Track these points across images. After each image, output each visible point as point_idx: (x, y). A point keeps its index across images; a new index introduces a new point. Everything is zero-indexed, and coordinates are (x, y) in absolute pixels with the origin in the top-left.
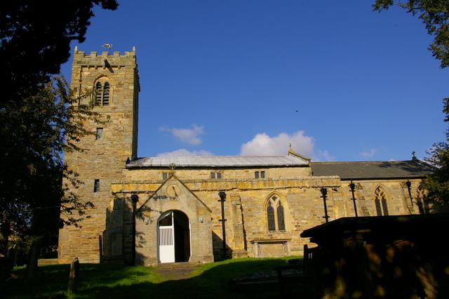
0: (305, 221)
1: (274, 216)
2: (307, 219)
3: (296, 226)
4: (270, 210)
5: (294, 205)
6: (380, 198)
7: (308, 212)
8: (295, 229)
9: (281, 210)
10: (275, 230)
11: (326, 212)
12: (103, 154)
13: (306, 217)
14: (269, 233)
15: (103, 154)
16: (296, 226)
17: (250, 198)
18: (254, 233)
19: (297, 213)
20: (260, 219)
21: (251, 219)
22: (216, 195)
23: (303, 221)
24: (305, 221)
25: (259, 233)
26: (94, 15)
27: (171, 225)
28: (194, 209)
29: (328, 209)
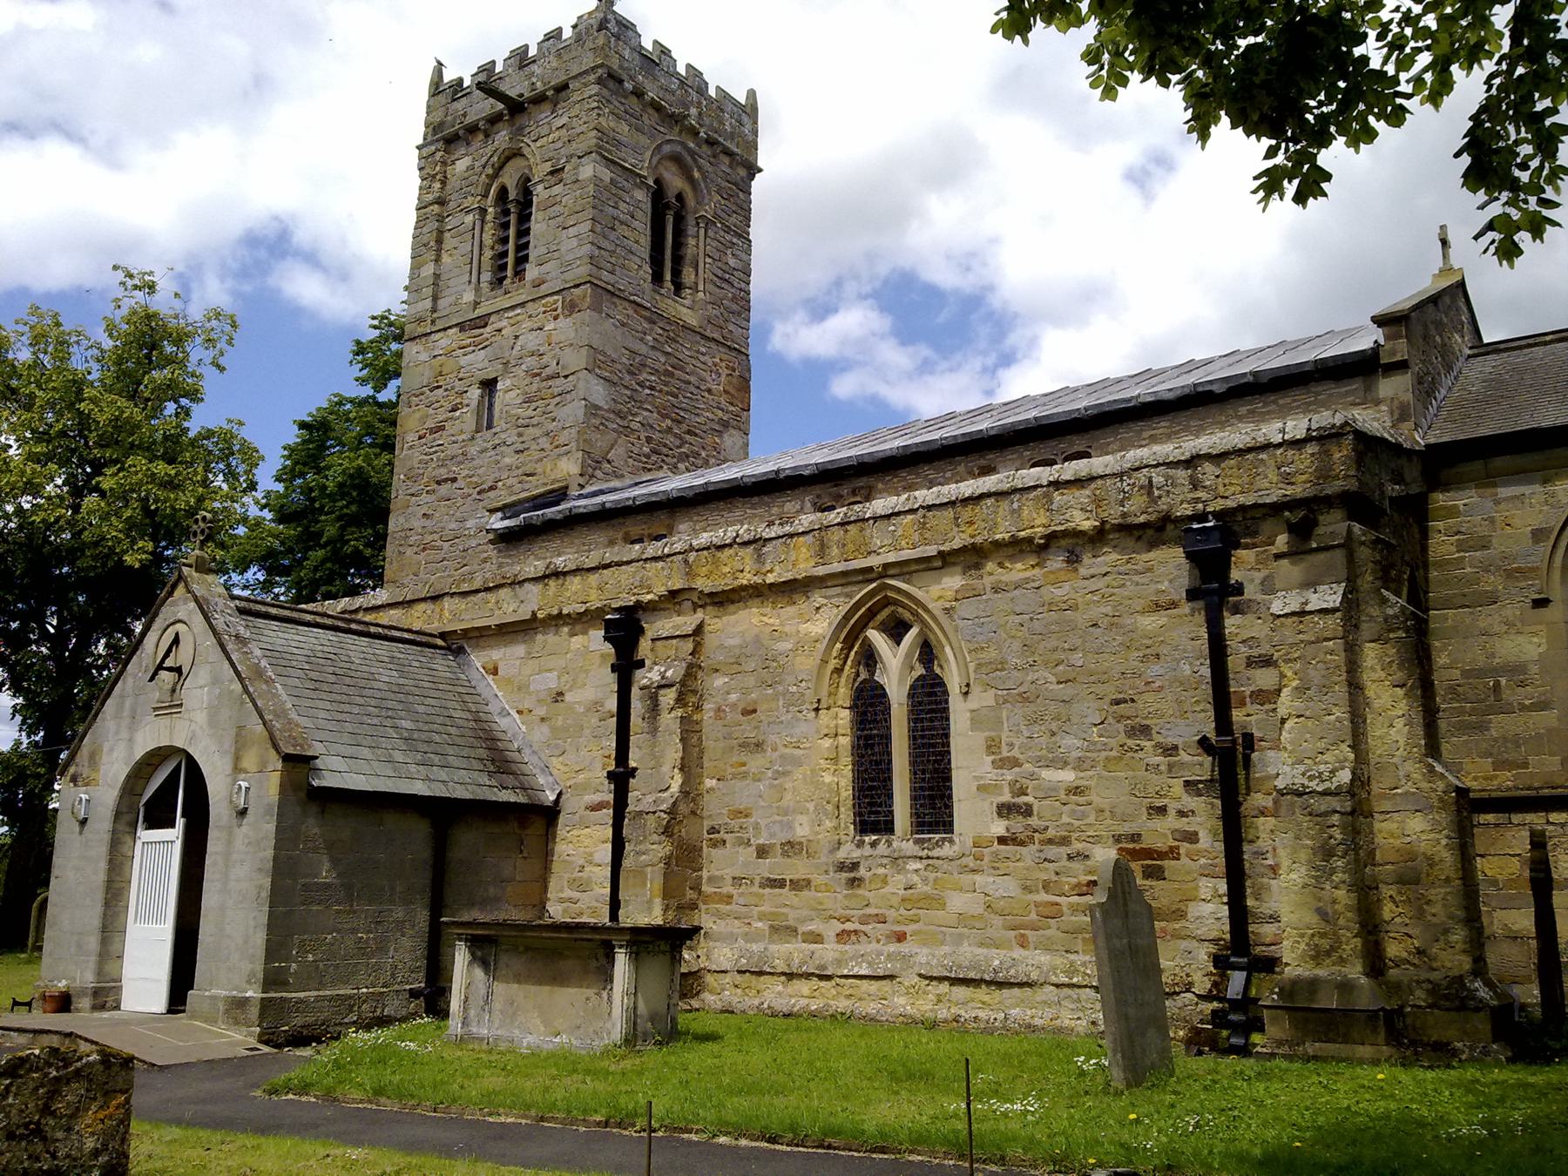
0: (1068, 776)
1: (887, 738)
2: (1080, 764)
3: (1005, 810)
4: (869, 704)
5: (1001, 665)
6: (896, 667)
7: (1090, 710)
8: (999, 828)
9: (930, 698)
10: (888, 828)
11: (1222, 700)
12: (491, 488)
13: (1070, 744)
14: (848, 852)
15: (491, 488)
16: (1005, 810)
17: (757, 639)
18: (762, 852)
19: (1012, 716)
20: (798, 762)
21: (756, 763)
22: (1170, 567)
23: (1050, 775)
24: (1068, 776)
25: (791, 847)
26: (1026, 42)
27: (173, 826)
28: (228, 743)
29: (1243, 681)
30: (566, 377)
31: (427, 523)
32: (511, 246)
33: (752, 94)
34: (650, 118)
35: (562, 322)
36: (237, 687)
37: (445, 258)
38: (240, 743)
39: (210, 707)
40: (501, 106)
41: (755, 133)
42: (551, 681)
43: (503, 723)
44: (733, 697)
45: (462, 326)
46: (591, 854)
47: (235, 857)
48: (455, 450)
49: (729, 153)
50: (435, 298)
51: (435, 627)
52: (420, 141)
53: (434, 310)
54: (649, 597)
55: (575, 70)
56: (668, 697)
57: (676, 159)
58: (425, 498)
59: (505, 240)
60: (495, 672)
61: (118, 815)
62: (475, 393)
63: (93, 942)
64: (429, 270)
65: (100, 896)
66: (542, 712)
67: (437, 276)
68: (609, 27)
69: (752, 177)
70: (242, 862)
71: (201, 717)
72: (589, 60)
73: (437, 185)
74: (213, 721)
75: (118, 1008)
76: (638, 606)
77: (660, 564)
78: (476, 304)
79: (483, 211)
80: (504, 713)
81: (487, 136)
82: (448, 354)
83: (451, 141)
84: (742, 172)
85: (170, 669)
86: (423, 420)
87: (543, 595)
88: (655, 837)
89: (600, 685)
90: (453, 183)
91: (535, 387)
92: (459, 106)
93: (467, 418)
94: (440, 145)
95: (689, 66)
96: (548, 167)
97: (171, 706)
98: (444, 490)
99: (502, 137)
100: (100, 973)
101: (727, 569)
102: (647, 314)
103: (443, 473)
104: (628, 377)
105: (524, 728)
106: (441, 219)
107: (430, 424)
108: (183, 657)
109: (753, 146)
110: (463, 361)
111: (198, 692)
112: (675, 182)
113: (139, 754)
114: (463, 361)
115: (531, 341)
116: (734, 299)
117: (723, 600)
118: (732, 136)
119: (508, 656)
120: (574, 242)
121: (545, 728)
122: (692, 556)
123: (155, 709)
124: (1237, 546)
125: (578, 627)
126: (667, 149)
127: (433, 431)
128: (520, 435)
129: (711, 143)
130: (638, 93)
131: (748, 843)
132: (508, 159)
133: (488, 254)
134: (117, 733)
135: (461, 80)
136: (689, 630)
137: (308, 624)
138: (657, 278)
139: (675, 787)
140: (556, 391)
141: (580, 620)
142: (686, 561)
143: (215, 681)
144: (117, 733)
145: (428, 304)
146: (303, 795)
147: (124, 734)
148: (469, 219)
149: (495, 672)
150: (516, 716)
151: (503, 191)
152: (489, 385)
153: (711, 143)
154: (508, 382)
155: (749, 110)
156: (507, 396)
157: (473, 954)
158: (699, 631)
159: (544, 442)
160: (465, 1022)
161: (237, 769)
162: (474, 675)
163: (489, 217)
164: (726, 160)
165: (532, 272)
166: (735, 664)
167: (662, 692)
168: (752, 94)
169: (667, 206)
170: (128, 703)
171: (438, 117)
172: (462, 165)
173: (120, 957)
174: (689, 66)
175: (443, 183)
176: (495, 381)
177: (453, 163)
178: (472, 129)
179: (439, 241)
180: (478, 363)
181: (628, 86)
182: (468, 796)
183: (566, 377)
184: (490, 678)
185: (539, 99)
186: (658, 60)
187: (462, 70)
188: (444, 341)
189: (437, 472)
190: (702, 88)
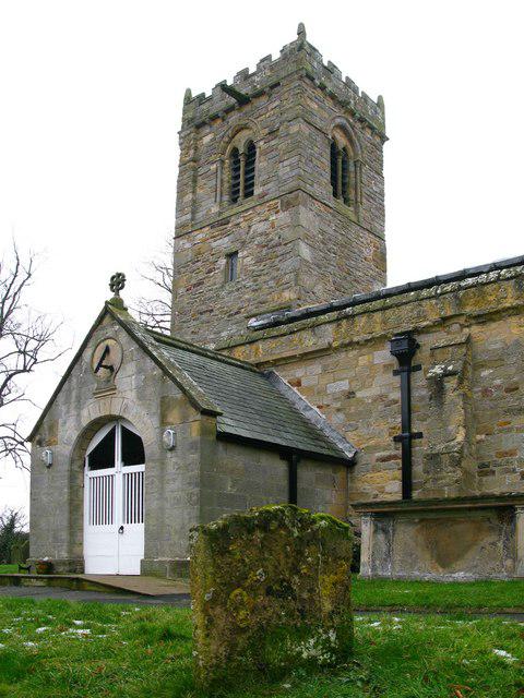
12: (237, 313)
15: (237, 313)
28: (155, 408)
30: (286, 244)
31: (195, 336)
32: (242, 179)
33: (380, 98)
34: (329, 103)
35: (281, 215)
36: (158, 372)
37: (199, 191)
38: (165, 407)
39: (138, 388)
40: (233, 100)
41: (384, 119)
42: (344, 386)
43: (307, 414)
44: (498, 382)
45: (212, 226)
46: (383, 487)
47: (167, 477)
48: (211, 294)
49: (372, 128)
50: (193, 213)
51: (252, 360)
52: (180, 129)
53: (193, 219)
54: (425, 323)
55: (283, 74)
56: (451, 384)
57: (342, 127)
58: (193, 323)
59: (238, 177)
60: (298, 384)
61: (72, 461)
62: (223, 261)
63: (64, 535)
64: (189, 197)
65: (66, 508)
66: (339, 405)
67: (194, 201)
68: (300, 50)
69: (383, 142)
70: (174, 480)
71: (131, 395)
72: (292, 68)
73: (192, 152)
74: (141, 396)
75: (83, 572)
76: (417, 331)
77: (434, 301)
78: (220, 213)
79: (223, 162)
80: (307, 408)
81: (223, 120)
82: (204, 241)
83: (198, 127)
84: (378, 140)
85: (105, 367)
86: (188, 281)
87: (337, 332)
88: (450, 468)
89: (385, 385)
90: (202, 149)
91: (264, 252)
92: (204, 107)
93: (218, 276)
94: (192, 129)
95: (347, 78)
96: (267, 131)
97: (108, 388)
98: (204, 317)
99: (234, 118)
100: (70, 551)
101: (491, 298)
102: (331, 211)
103: (204, 308)
104: (322, 246)
105: (324, 416)
106: (195, 169)
107: (194, 281)
108: (114, 358)
109: (383, 125)
110: (214, 244)
111: (128, 380)
112: (342, 141)
113: (85, 422)
114: (214, 244)
115: (261, 227)
116: (377, 209)
117: (483, 319)
118: (372, 118)
119: (310, 373)
120: (288, 169)
121: (341, 416)
122: (461, 293)
123: (95, 394)
124: (77, 563)
125: (364, 350)
126: (338, 121)
127: (195, 286)
128: (255, 281)
129: (361, 120)
130: (323, 88)
131: (514, 471)
132: (238, 132)
133: (226, 185)
134: (68, 412)
135: (203, 94)
136: (463, 339)
137: (183, 349)
138: (335, 194)
139: (460, 438)
140: (279, 253)
141: (373, 342)
142: (456, 297)
143: (140, 371)
144: (68, 412)
145: (189, 216)
146: (213, 437)
147: (73, 412)
148: (213, 167)
149: (298, 384)
150: (317, 410)
151: (235, 150)
152: (232, 255)
153: (361, 120)
154: (245, 253)
155: (380, 104)
156: (246, 259)
157: (376, 526)
158: (469, 340)
159: (272, 283)
160: (374, 568)
161: (163, 422)
162: (283, 389)
163: (226, 165)
164: (370, 131)
165: (257, 191)
166: (498, 360)
167: (446, 379)
168: (380, 98)
169: (338, 153)
170: (74, 394)
171: (190, 115)
172: (207, 139)
173: (81, 544)
174: (347, 78)
175: (196, 149)
176: (236, 253)
177: (201, 138)
178: (214, 118)
179: (195, 181)
180: (224, 244)
181: (317, 82)
182: (305, 449)
183: (286, 244)
184: (295, 389)
185: (261, 94)
186: (330, 70)
187: (205, 87)
188: (200, 236)
189: (200, 308)
190: (355, 90)
